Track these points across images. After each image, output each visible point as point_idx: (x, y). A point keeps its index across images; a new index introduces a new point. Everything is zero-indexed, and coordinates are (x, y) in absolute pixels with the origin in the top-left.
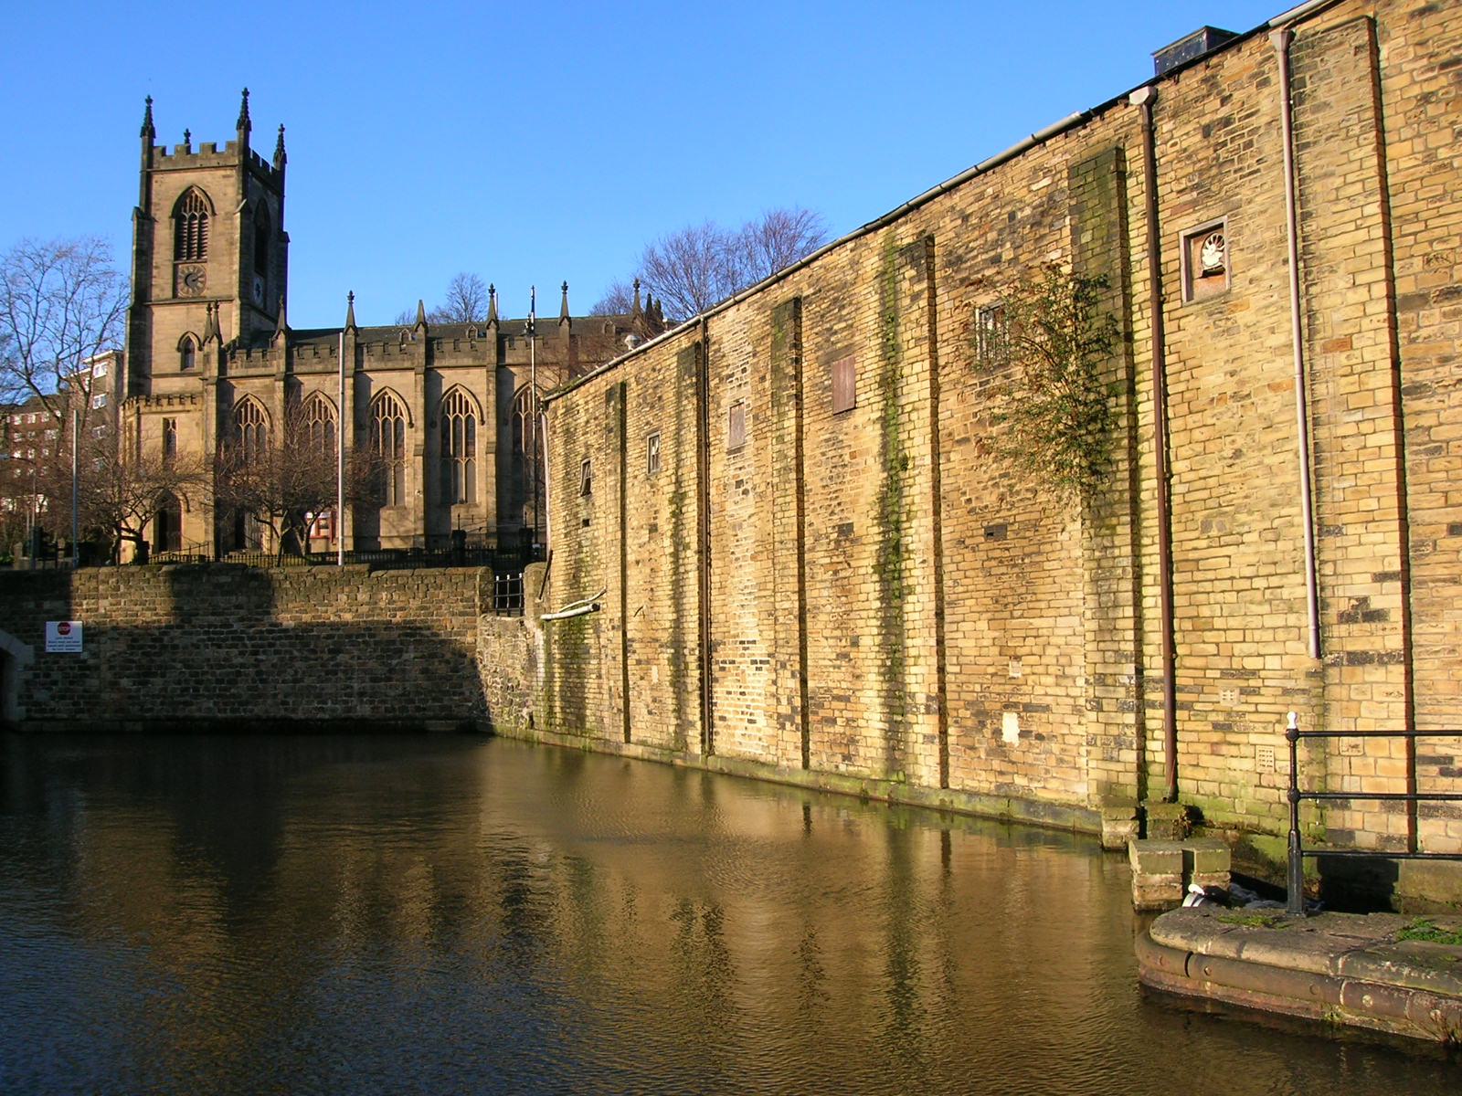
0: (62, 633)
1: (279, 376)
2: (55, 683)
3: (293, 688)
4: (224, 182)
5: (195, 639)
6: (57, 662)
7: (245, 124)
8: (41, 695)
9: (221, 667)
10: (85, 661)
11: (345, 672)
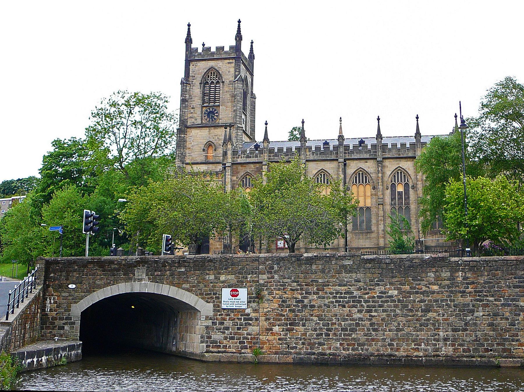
0: (233, 296)
2: (227, 328)
7: (239, 37)
8: (217, 336)
9: (345, 320)
10: (248, 315)
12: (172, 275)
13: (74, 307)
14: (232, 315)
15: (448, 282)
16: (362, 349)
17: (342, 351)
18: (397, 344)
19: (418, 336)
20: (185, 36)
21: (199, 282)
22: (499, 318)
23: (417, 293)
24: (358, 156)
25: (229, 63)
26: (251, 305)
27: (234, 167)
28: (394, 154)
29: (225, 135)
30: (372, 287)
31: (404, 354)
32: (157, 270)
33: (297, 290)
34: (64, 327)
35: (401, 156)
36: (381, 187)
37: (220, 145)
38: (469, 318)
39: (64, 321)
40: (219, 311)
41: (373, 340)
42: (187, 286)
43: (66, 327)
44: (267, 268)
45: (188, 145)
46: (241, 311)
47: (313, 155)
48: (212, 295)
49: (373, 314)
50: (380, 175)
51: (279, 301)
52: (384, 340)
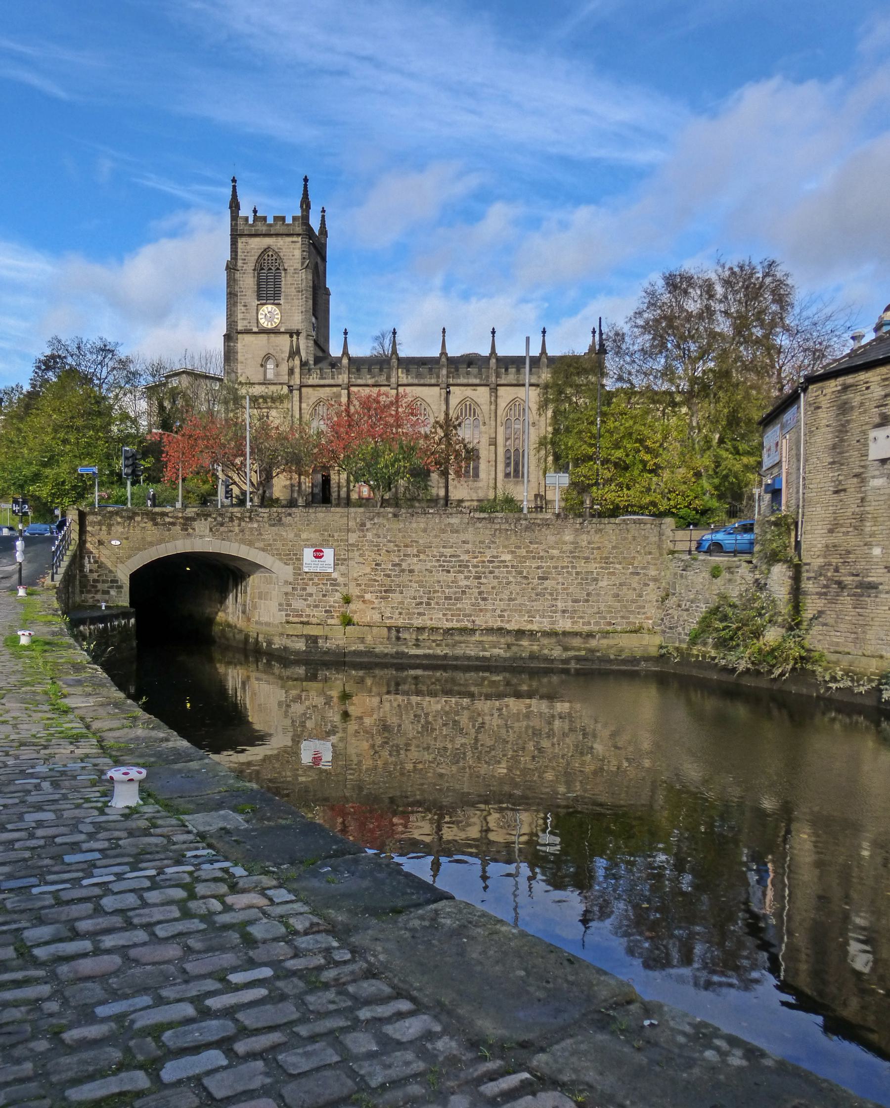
0: (316, 557)
1: (344, 386)
2: (311, 595)
3: (509, 605)
4: (293, 246)
5: (429, 565)
6: (312, 579)
8: (298, 604)
9: (449, 587)
10: (335, 580)
11: (551, 594)
14: (316, 580)
21: (275, 540)
23: (534, 558)
24: (465, 381)
25: (293, 242)
27: (304, 390)
29: (292, 346)
37: (283, 359)
38: (591, 588)
39: (110, 584)
40: (300, 575)
42: (261, 545)
43: (113, 592)
50: (493, 407)
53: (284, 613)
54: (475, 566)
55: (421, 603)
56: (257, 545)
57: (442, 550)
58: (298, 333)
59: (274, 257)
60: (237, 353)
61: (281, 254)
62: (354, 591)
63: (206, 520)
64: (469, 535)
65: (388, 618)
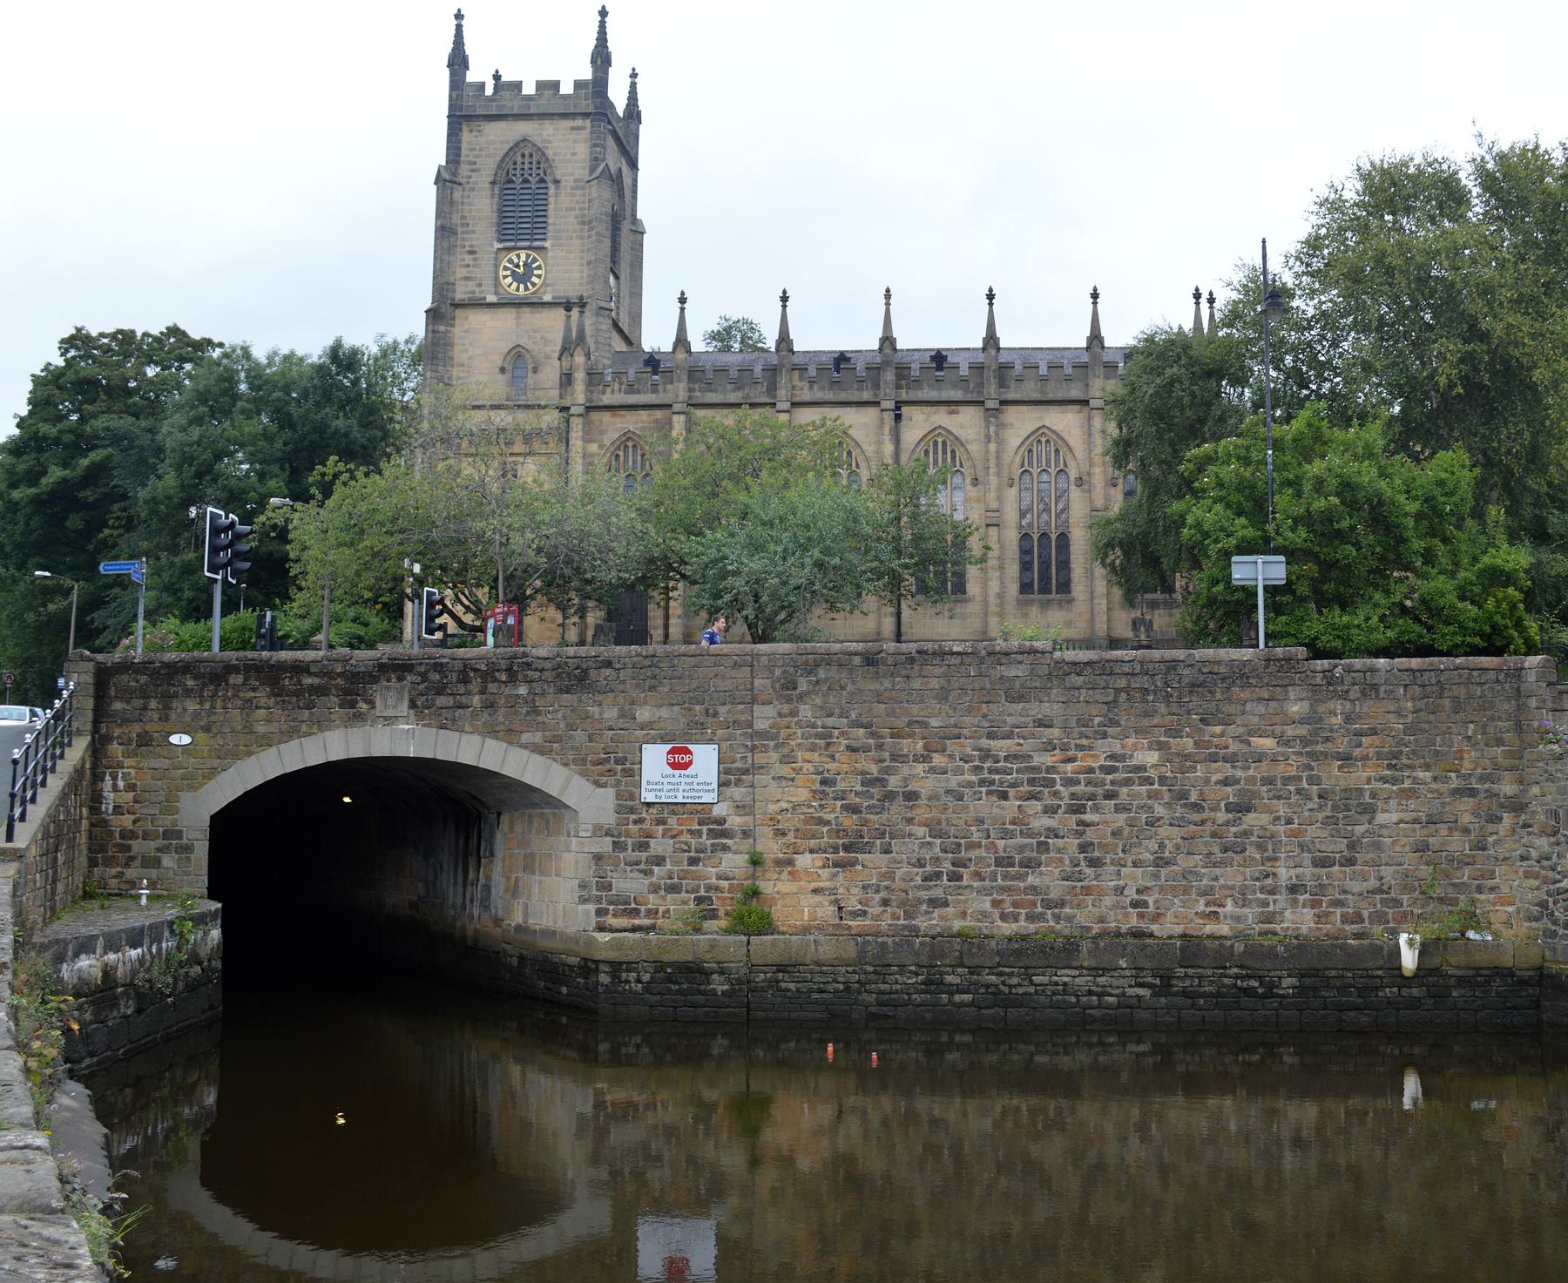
0: (674, 766)
2: (660, 861)
3: (1156, 876)
4: (574, 135)
7: (601, 57)
8: (629, 884)
9: (1006, 834)
10: (721, 821)
12: (490, 706)
13: (187, 801)
14: (672, 821)
15: (1302, 730)
16: (1057, 918)
17: (999, 923)
18: (1156, 901)
19: (1216, 879)
20: (448, 47)
21: (571, 727)
22: (1443, 829)
23: (1213, 758)
24: (933, 395)
25: (573, 128)
26: (729, 791)
27: (595, 416)
28: (1030, 390)
29: (568, 329)
30: (1084, 742)
31: (1178, 930)
32: (436, 687)
33: (867, 749)
34: (159, 861)
35: (1050, 396)
36: (993, 479)
37: (548, 357)
38: (1359, 829)
39: (160, 842)
40: (632, 811)
41: (1087, 891)
42: (537, 737)
43: (168, 861)
44: (778, 686)
45: (458, 354)
46: (700, 812)
47: (811, 388)
48: (612, 765)
49: (1088, 817)
50: (993, 447)
51: (813, 782)
52: (1120, 891)
53: (591, 907)
54: (1070, 782)
55: (938, 875)
56: (526, 737)
57: (985, 742)
58: (582, 304)
59: (535, 159)
60: (452, 345)
61: (549, 153)
62: (771, 847)
63: (400, 679)
64: (1049, 708)
65: (856, 914)
